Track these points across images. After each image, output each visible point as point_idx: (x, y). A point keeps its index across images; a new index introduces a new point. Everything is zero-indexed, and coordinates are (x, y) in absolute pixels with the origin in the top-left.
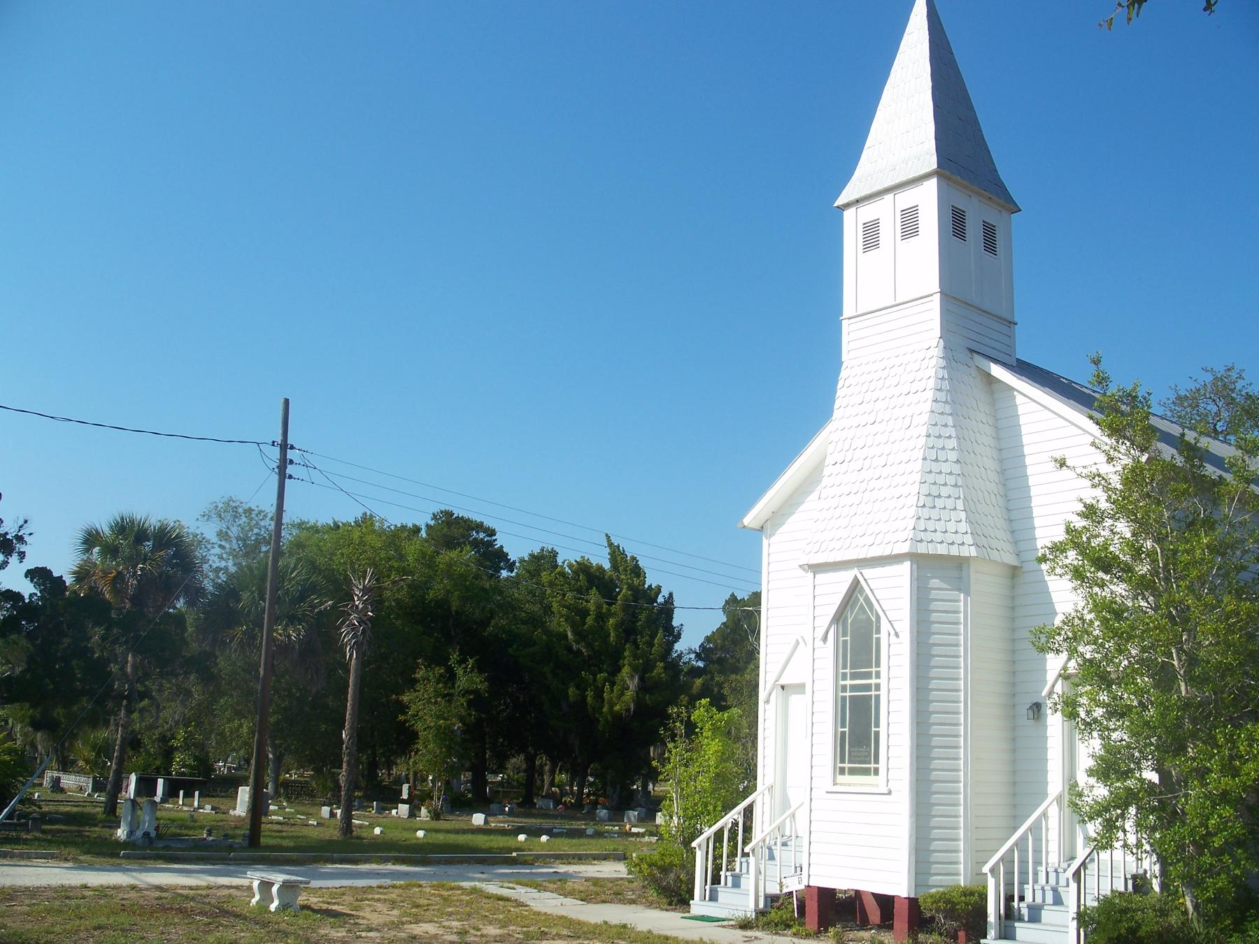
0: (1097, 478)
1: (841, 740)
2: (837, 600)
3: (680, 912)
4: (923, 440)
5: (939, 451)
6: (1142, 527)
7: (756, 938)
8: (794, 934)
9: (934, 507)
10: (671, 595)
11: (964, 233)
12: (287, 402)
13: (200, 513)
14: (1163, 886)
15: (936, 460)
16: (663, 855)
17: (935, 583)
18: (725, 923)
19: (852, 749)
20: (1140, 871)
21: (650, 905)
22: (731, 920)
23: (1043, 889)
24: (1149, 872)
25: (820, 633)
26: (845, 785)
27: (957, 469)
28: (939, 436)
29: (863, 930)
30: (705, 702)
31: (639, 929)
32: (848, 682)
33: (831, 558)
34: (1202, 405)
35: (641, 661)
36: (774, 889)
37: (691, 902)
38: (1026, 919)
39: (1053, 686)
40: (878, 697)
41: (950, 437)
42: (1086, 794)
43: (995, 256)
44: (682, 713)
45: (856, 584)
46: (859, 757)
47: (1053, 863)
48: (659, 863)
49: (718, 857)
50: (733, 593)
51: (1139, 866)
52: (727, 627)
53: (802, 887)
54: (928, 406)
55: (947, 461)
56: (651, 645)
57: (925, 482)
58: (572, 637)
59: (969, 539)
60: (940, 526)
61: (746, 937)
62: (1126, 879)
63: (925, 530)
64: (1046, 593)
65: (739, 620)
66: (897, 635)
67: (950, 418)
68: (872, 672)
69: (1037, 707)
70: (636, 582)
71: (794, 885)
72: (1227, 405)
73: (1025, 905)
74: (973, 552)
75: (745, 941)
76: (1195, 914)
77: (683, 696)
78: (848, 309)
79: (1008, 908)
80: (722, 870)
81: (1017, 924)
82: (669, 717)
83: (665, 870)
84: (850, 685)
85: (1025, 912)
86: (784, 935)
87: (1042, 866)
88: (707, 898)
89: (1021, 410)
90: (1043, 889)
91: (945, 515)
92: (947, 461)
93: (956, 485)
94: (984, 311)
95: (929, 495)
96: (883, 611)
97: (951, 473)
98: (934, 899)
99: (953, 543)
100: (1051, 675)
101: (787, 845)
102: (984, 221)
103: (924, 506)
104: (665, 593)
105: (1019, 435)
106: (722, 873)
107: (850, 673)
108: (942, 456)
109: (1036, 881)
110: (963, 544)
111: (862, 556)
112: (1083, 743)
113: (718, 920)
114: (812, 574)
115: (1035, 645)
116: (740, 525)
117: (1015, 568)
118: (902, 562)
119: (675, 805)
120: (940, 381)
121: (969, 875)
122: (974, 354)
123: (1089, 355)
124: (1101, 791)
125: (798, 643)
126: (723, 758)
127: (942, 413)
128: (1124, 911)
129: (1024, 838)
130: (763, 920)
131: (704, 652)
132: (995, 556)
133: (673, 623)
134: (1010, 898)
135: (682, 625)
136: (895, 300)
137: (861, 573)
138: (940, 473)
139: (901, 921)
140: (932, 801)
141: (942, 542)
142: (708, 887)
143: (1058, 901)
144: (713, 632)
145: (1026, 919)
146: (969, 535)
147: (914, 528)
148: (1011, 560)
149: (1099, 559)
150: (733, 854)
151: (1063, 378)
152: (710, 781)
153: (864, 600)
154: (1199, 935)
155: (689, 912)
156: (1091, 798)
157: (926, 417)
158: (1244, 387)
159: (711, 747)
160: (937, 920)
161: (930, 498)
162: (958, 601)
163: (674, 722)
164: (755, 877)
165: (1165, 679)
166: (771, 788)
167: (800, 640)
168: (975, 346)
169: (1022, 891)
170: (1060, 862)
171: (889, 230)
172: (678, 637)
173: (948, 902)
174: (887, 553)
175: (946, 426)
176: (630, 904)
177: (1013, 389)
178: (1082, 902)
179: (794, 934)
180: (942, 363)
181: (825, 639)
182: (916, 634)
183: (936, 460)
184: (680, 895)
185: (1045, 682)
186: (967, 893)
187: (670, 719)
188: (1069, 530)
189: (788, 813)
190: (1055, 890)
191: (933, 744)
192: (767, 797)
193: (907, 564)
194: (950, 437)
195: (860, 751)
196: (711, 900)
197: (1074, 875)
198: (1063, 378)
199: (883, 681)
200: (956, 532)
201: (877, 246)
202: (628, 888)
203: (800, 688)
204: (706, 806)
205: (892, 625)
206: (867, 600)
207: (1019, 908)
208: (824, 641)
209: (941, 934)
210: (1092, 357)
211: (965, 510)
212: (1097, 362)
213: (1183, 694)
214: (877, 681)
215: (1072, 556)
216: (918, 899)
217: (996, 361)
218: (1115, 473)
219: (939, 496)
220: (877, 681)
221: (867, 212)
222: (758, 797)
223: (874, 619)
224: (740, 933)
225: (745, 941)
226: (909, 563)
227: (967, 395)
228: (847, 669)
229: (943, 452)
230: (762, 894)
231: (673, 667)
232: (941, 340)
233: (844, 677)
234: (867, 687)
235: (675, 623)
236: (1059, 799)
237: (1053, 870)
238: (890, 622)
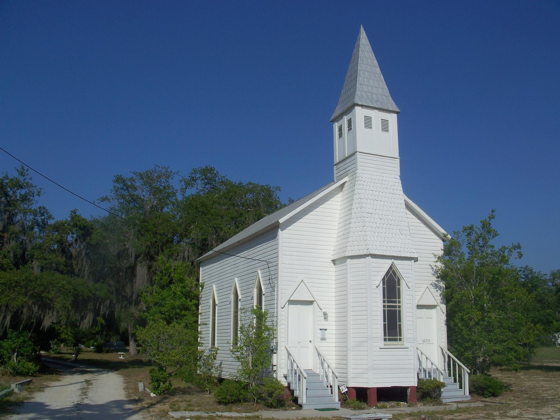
12: (416, 260)
32: (386, 304)
33: (403, 255)
58: (8, 316)
164: (413, 258)
201: (417, 308)
214: (399, 304)
220: (399, 304)
234: (395, 307)
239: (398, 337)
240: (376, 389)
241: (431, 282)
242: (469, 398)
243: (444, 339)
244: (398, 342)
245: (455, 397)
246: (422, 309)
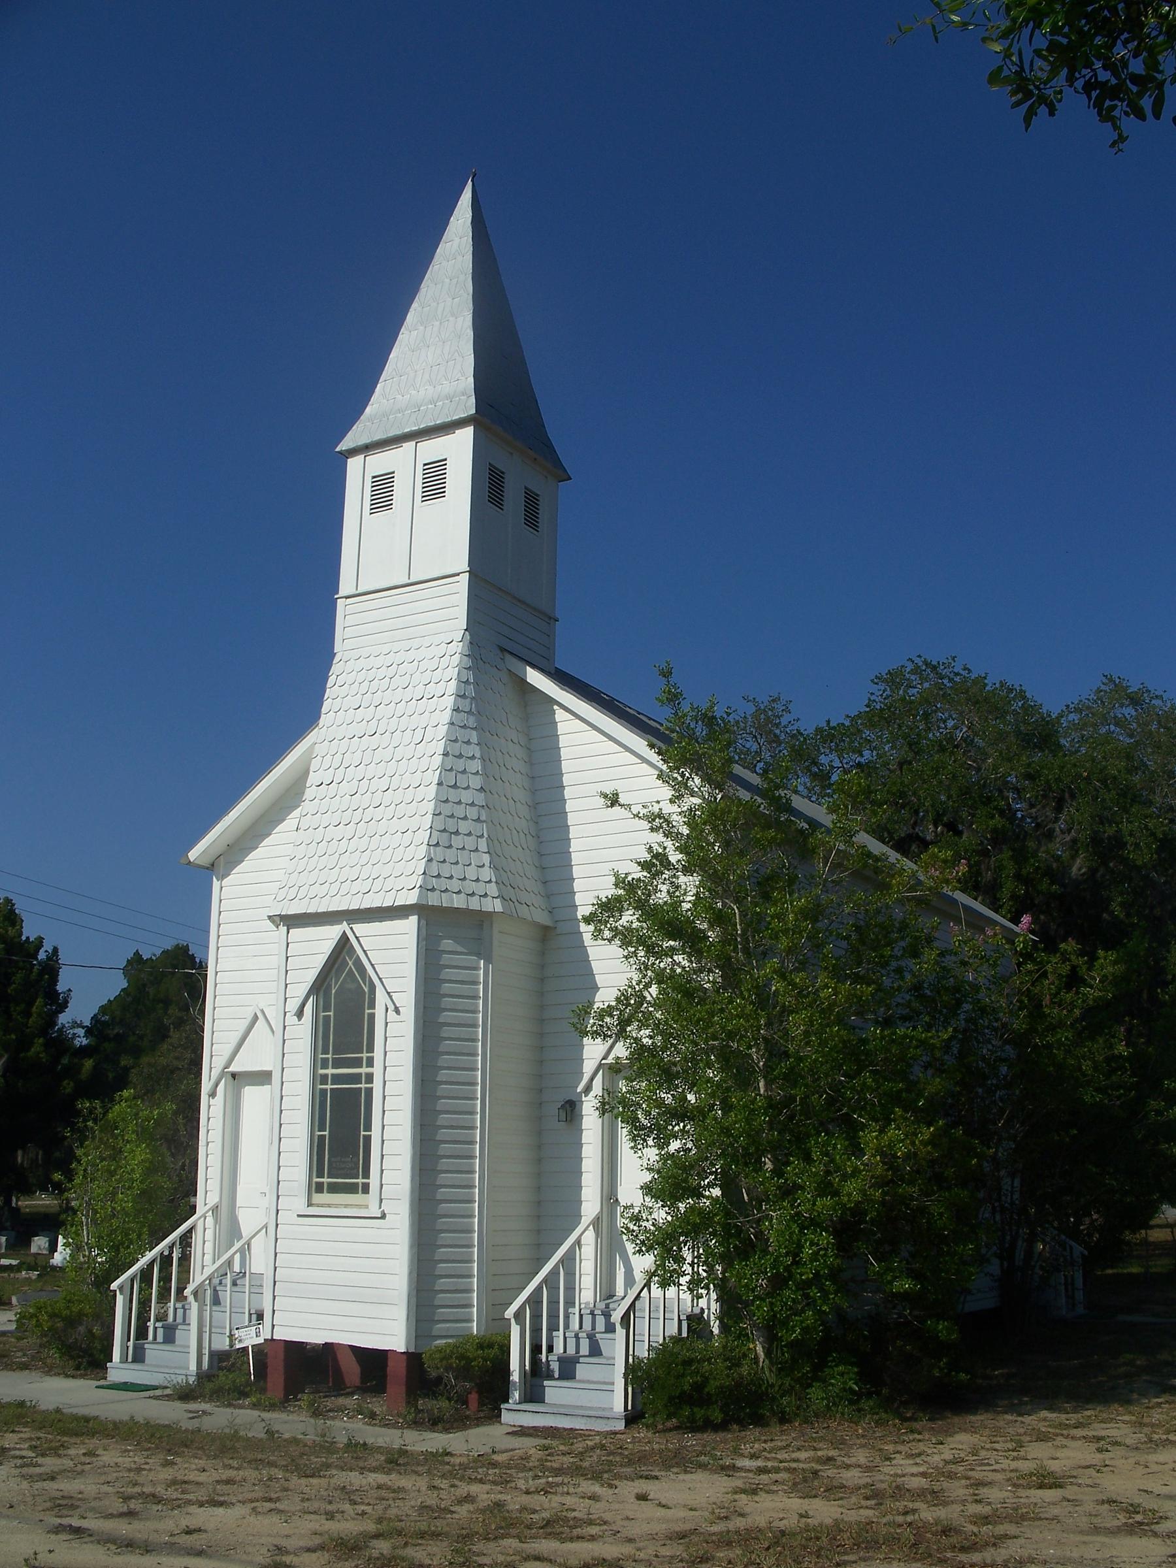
0: (657, 820)
1: (317, 1149)
2: (320, 961)
3: (92, 1379)
4: (438, 759)
5: (459, 775)
6: (714, 880)
7: (204, 1412)
8: (254, 1405)
9: (450, 846)
10: (55, 950)
11: (502, 500)
13: (927, 658)
14: (724, 1327)
15: (455, 786)
16: (69, 1301)
17: (447, 944)
18: (158, 1392)
19: (333, 1159)
20: (697, 1311)
21: (49, 1370)
22: (166, 1387)
23: (577, 1337)
24: (706, 1311)
25: (293, 1005)
26: (322, 1206)
27: (480, 799)
28: (460, 756)
29: (342, 1395)
30: (127, 1094)
31: (43, 1407)
32: (330, 1071)
34: (740, 741)
35: (13, 1037)
36: (222, 1344)
37: (109, 1365)
38: (556, 1375)
39: (592, 1079)
40: (369, 1092)
41: (473, 758)
42: (644, 1218)
43: (535, 532)
44: (96, 1108)
45: (344, 941)
46: (343, 1169)
47: (587, 1303)
48: (65, 1313)
49: (144, 1304)
50: (137, 951)
51: (695, 1305)
52: (128, 995)
53: (260, 1340)
54: (446, 716)
55: (468, 787)
56: (28, 1014)
57: (440, 814)
59: (493, 890)
60: (457, 871)
61: (191, 1412)
62: (680, 1321)
63: (439, 876)
64: (586, 960)
65: (144, 985)
66: (397, 1011)
67: (474, 733)
68: (362, 1058)
69: (571, 1107)
70: (11, 932)
71: (249, 1338)
72: (770, 743)
73: (556, 1358)
74: (498, 906)
75: (191, 1418)
76: (767, 1361)
77: (66, 1082)
78: (346, 585)
79: (535, 1361)
80: (150, 1321)
81: (546, 1383)
82: (78, 1113)
83: (72, 1322)
84: (332, 1075)
85: (555, 1366)
86: (241, 1407)
87: (575, 1307)
88: (130, 1359)
89: (561, 728)
90: (577, 1337)
91: (463, 857)
92: (468, 787)
93: (478, 820)
94: (519, 601)
95: (444, 830)
96: (380, 979)
97: (472, 804)
98: (443, 1354)
99: (473, 894)
100: (589, 1067)
102: (526, 488)
103: (437, 844)
104: (47, 947)
105: (558, 761)
106: (151, 1324)
107: (333, 1058)
108: (462, 781)
109: (567, 1326)
110: (486, 895)
111: (354, 906)
112: (635, 1152)
113: (147, 1388)
114: (286, 928)
115: (577, 1029)
116: (183, 861)
117: (546, 928)
118: (406, 916)
119: (85, 1233)
120: (463, 684)
121: (484, 1322)
122: (505, 653)
123: (657, 665)
124: (661, 1215)
125: (256, 1018)
126: (151, 1169)
127: (464, 727)
128: (688, 1362)
129: (554, 1272)
130: (209, 1386)
131: (96, 1028)
132: (524, 911)
133: (58, 988)
134: (536, 1349)
135: (70, 990)
136: (409, 578)
137: (351, 928)
138: (460, 803)
139: (396, 1388)
140: (438, 1227)
141: (459, 892)
142: (131, 1344)
143: (595, 1351)
144: (109, 1000)
145: (556, 1375)
146: (493, 884)
147: (424, 873)
148: (542, 918)
149: (670, 923)
150: (164, 1296)
151: (605, 694)
152: (134, 1201)
153: (353, 964)
154: (772, 1386)
155: (105, 1378)
156: (651, 1222)
157: (443, 730)
158: (790, 722)
159: (137, 1156)
160: (445, 1380)
161: (445, 835)
162: (477, 968)
163: (85, 1121)
165: (742, 1076)
166: (215, 1209)
167: (259, 1015)
168: (508, 645)
169: (550, 1339)
170: (595, 1301)
171: (405, 489)
172: (63, 1006)
173: (462, 1357)
174: (388, 903)
175: (468, 743)
176: (22, 1369)
177: (552, 701)
178: (631, 1352)
179: (254, 1405)
180: (468, 662)
181: (300, 1014)
182: (422, 1010)
183: (455, 786)
184: (91, 1355)
185: (581, 1074)
186: (483, 1344)
187: (80, 1116)
188: (620, 882)
189: (237, 1245)
190: (591, 1337)
191: (441, 1152)
192: (210, 1220)
193: (414, 919)
194: (473, 758)
195: (344, 1162)
196: (134, 1361)
197: (622, 1318)
198: (605, 694)
199: (377, 1070)
200: (477, 880)
201: (389, 506)
202: (15, 1347)
203: (263, 1078)
204: (127, 1235)
205: (391, 997)
206: (358, 964)
207: (548, 1361)
208: (298, 1017)
209: (449, 1399)
210: (661, 668)
211: (488, 852)
212: (666, 674)
213: (762, 1091)
214: (369, 1070)
215: (629, 917)
216: (421, 1354)
217: (534, 666)
218: (680, 814)
219: (457, 833)
220: (369, 1070)
221: (379, 462)
222: (199, 1222)
223: (366, 990)
224: (179, 1405)
225: (191, 1418)
227: (495, 706)
228: (328, 1054)
229: (464, 776)
230: (206, 1351)
231: (60, 1044)
232: (467, 633)
233: (325, 1064)
234: (356, 1078)
235: (61, 987)
236: (596, 1223)
237: (589, 1312)
238: (388, 993)
240: (282, 1344)
245: (562, 1411)
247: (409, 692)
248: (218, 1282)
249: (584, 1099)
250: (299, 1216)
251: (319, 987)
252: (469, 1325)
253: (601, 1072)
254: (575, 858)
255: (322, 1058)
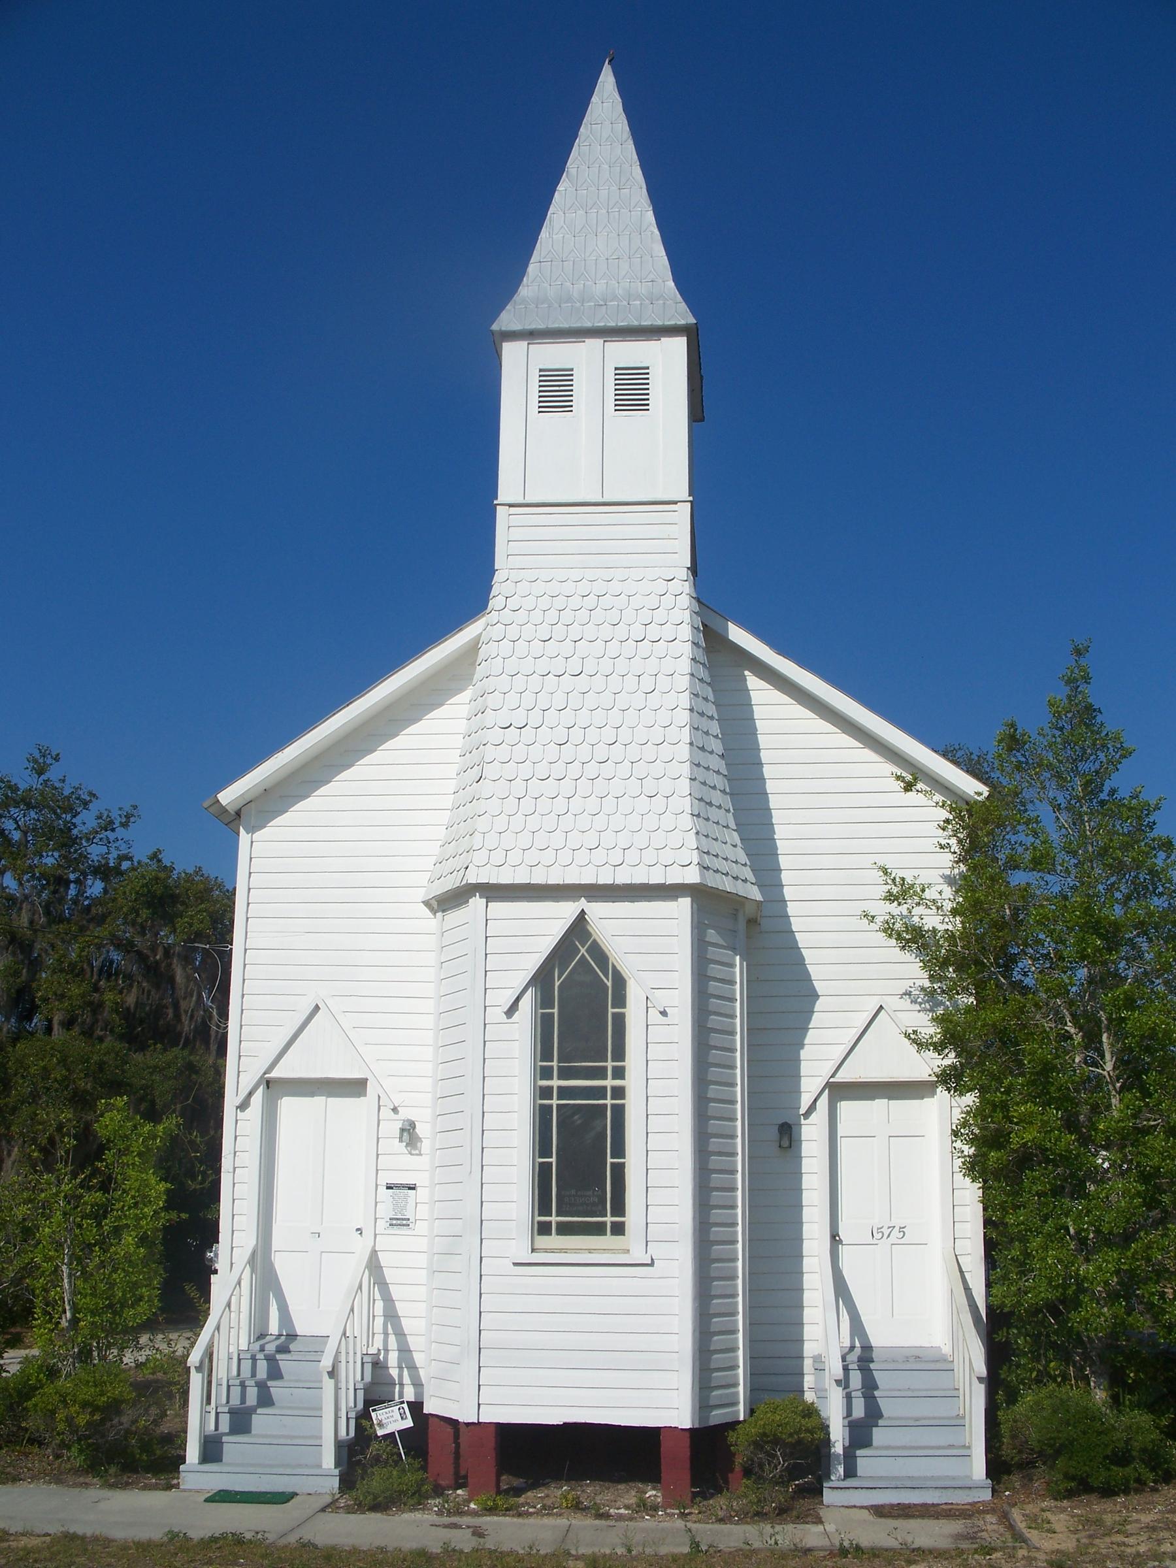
32: (555, 1083)
39: (250, 1094)
40: (619, 1112)
78: (508, 488)
101: (290, 1352)
107: (559, 1067)
118: (674, 898)
153: (587, 951)
162: (732, 966)
181: (511, 1010)
214: (618, 1083)
220: (618, 1083)
223: (609, 984)
226: (689, 900)
234: (600, 1092)
239: (609, 1219)
240: (493, 1428)
241: (904, 986)
242: (986, 1495)
243: (968, 1226)
244: (608, 1240)
246: (873, 1098)
247: (621, 631)
248: (258, 1348)
249: (803, 1121)
250: (515, 1264)
251: (541, 979)
252: (732, 1390)
253: (827, 1091)
254: (782, 846)
255: (541, 1066)
